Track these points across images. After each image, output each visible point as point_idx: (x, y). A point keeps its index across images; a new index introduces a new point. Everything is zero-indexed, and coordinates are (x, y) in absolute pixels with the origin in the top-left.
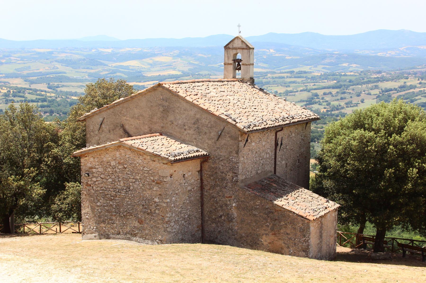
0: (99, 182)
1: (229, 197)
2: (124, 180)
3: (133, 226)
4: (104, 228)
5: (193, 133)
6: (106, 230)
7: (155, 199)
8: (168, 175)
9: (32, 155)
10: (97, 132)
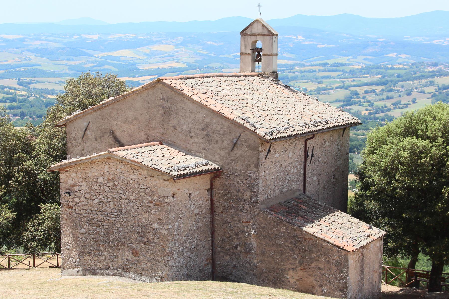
0: (82, 203)
1: (247, 222)
4: (90, 262)
5: (201, 141)
6: (91, 264)
7: (153, 225)
8: (170, 194)
10: (80, 141)
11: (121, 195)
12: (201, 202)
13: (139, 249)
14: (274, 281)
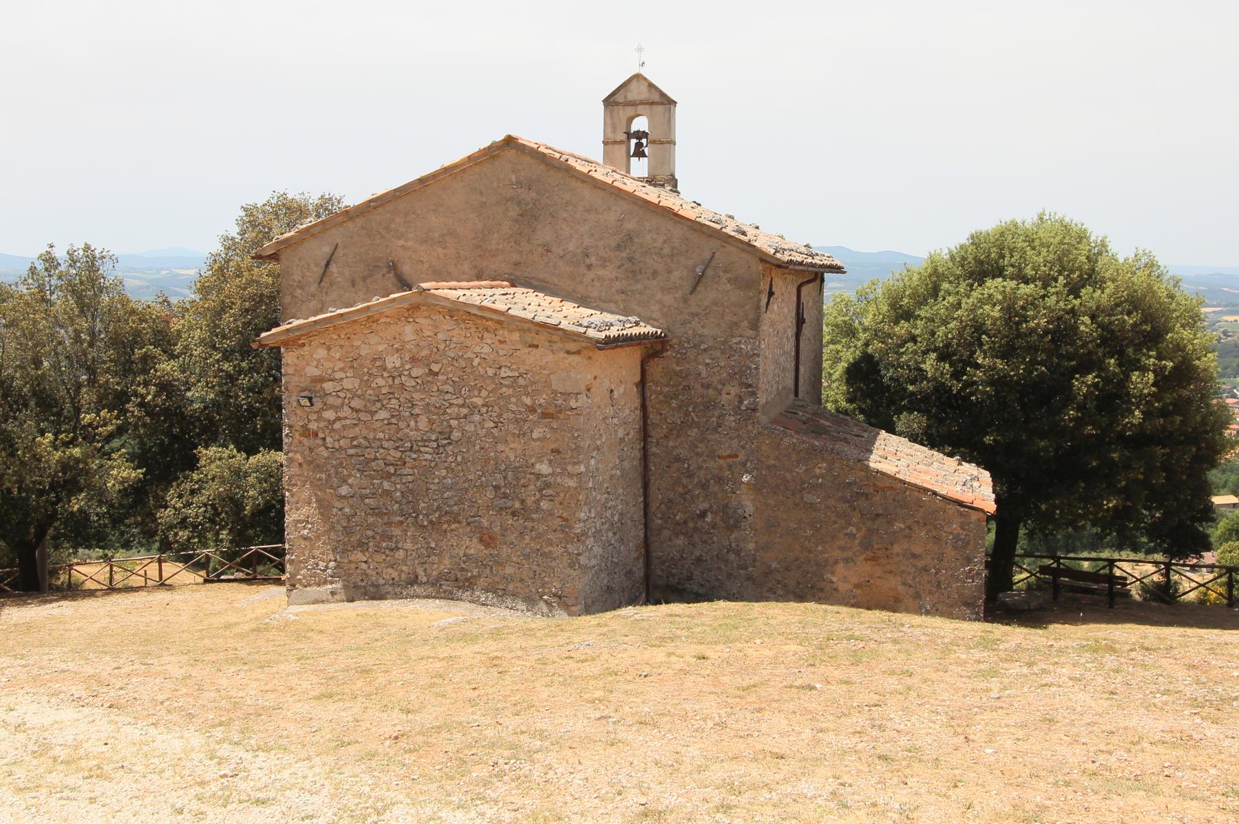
0: (343, 422)
1: (730, 456)
2: (429, 411)
3: (461, 554)
4: (364, 566)
5: (614, 274)
6: (369, 572)
7: (538, 466)
8: (583, 388)
9: (102, 380)
10: (313, 288)
11: (448, 396)
12: (627, 412)
13: (497, 529)
14: (797, 591)
